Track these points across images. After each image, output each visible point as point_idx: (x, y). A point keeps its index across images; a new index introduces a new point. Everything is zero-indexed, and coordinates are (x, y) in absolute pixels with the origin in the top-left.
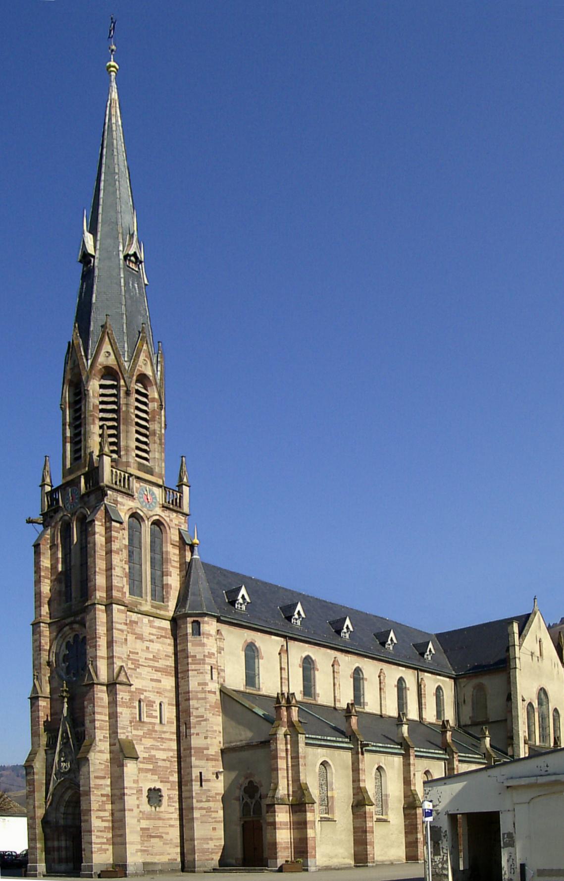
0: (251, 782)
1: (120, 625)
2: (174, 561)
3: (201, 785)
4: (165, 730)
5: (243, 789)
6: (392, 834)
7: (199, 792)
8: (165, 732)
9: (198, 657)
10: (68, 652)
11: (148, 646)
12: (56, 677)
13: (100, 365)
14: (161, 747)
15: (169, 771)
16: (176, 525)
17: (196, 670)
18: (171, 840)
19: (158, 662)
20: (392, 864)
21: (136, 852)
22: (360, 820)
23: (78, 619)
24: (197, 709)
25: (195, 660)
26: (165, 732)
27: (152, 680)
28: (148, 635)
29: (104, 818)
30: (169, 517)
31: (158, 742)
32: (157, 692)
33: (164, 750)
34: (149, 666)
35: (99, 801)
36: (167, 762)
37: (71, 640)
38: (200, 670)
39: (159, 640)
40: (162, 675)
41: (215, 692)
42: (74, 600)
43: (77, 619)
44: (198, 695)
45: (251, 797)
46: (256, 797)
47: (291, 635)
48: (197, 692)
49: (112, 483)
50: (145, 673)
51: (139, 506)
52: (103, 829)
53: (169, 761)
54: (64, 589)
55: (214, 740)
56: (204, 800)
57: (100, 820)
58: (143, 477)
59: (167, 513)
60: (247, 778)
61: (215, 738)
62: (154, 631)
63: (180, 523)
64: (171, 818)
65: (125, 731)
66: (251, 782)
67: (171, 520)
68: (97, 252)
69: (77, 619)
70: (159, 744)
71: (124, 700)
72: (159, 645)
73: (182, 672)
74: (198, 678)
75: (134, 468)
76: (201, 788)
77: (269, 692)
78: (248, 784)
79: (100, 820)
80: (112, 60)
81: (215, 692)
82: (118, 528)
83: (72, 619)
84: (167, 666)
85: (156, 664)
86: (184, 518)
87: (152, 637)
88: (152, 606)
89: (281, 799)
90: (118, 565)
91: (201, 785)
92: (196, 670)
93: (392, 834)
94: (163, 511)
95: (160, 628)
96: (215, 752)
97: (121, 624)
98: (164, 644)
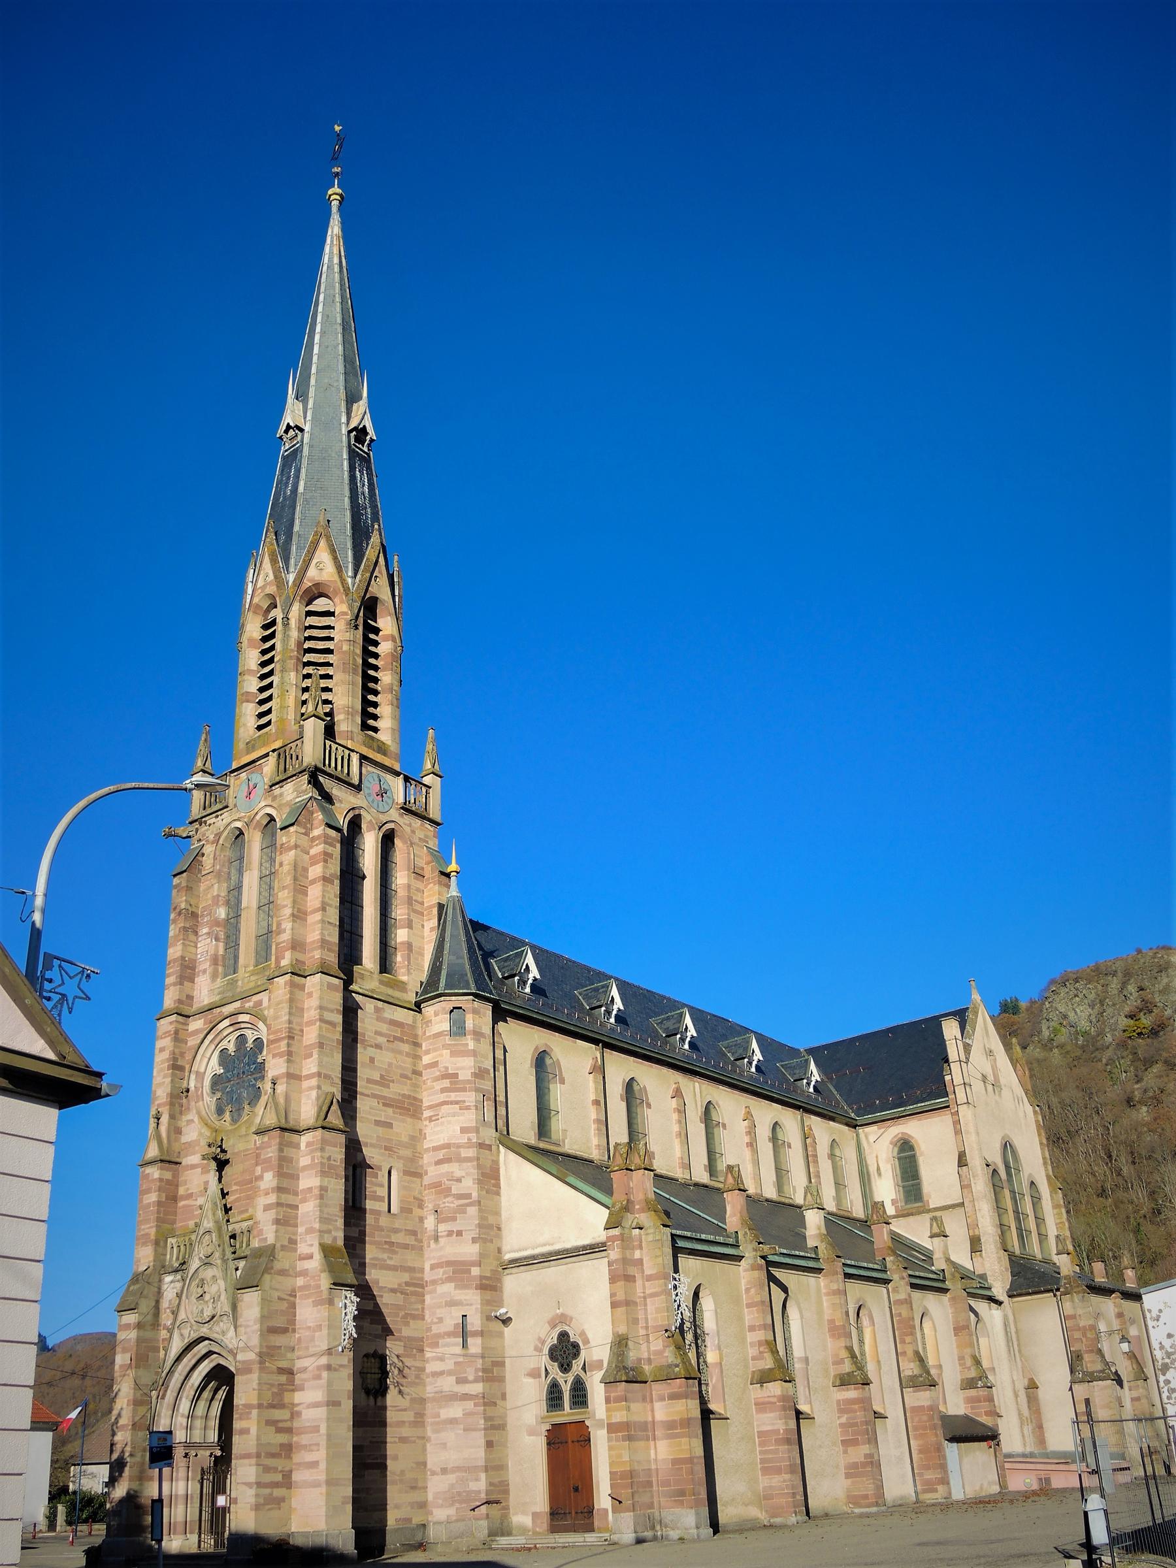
0: (563, 1336)
1: (330, 1014)
2: (416, 901)
3: (464, 1345)
4: (397, 1226)
5: (546, 1351)
6: (820, 1446)
7: (461, 1359)
8: (396, 1231)
9: (460, 1078)
10: (222, 1071)
11: (373, 1055)
12: (196, 1119)
13: (308, 580)
14: (389, 1262)
15: (402, 1313)
16: (420, 839)
17: (457, 1103)
18: (402, 1472)
19: (389, 1087)
20: (827, 1515)
21: (343, 1503)
22: (772, 1415)
23: (249, 1005)
24: (459, 1180)
25: (456, 1083)
26: (396, 1231)
27: (378, 1123)
28: (373, 1035)
29: (281, 1425)
30: (410, 825)
31: (384, 1250)
32: (386, 1148)
33: (394, 1268)
34: (374, 1096)
35: (272, 1385)
36: (398, 1294)
37: (231, 1048)
38: (464, 1101)
39: (390, 1045)
40: (394, 1113)
41: (491, 1146)
42: (241, 970)
43: (247, 1005)
44: (459, 1154)
45: (565, 1368)
46: (574, 1367)
47: (606, 1040)
48: (459, 1146)
49: (324, 765)
50: (367, 1108)
51: (364, 804)
52: (277, 1450)
53: (402, 1293)
54: (221, 951)
55: (488, 1244)
56: (471, 1378)
57: (273, 1429)
58: (371, 756)
59: (408, 819)
60: (554, 1327)
61: (491, 1241)
62: (384, 1028)
63: (426, 836)
64: (403, 1422)
65: (331, 1227)
66: (563, 1336)
67: (413, 832)
68: (308, 424)
69: (247, 1005)
70: (385, 1256)
71: (332, 1162)
72: (390, 1054)
73: (430, 1107)
74: (461, 1118)
75: (358, 741)
76: (463, 1352)
77: (575, 1147)
78: (559, 1338)
79: (273, 1429)
80: (336, 186)
81: (491, 1146)
82: (334, 838)
83: (237, 1005)
84: (404, 1095)
85: (385, 1092)
86: (432, 829)
87: (381, 1040)
88: (381, 982)
89: (632, 1369)
90: (331, 902)
91: (464, 1345)
92: (457, 1103)
93: (820, 1446)
94: (401, 815)
95: (393, 1023)
96: (492, 1270)
97: (332, 1011)
98: (400, 1052)
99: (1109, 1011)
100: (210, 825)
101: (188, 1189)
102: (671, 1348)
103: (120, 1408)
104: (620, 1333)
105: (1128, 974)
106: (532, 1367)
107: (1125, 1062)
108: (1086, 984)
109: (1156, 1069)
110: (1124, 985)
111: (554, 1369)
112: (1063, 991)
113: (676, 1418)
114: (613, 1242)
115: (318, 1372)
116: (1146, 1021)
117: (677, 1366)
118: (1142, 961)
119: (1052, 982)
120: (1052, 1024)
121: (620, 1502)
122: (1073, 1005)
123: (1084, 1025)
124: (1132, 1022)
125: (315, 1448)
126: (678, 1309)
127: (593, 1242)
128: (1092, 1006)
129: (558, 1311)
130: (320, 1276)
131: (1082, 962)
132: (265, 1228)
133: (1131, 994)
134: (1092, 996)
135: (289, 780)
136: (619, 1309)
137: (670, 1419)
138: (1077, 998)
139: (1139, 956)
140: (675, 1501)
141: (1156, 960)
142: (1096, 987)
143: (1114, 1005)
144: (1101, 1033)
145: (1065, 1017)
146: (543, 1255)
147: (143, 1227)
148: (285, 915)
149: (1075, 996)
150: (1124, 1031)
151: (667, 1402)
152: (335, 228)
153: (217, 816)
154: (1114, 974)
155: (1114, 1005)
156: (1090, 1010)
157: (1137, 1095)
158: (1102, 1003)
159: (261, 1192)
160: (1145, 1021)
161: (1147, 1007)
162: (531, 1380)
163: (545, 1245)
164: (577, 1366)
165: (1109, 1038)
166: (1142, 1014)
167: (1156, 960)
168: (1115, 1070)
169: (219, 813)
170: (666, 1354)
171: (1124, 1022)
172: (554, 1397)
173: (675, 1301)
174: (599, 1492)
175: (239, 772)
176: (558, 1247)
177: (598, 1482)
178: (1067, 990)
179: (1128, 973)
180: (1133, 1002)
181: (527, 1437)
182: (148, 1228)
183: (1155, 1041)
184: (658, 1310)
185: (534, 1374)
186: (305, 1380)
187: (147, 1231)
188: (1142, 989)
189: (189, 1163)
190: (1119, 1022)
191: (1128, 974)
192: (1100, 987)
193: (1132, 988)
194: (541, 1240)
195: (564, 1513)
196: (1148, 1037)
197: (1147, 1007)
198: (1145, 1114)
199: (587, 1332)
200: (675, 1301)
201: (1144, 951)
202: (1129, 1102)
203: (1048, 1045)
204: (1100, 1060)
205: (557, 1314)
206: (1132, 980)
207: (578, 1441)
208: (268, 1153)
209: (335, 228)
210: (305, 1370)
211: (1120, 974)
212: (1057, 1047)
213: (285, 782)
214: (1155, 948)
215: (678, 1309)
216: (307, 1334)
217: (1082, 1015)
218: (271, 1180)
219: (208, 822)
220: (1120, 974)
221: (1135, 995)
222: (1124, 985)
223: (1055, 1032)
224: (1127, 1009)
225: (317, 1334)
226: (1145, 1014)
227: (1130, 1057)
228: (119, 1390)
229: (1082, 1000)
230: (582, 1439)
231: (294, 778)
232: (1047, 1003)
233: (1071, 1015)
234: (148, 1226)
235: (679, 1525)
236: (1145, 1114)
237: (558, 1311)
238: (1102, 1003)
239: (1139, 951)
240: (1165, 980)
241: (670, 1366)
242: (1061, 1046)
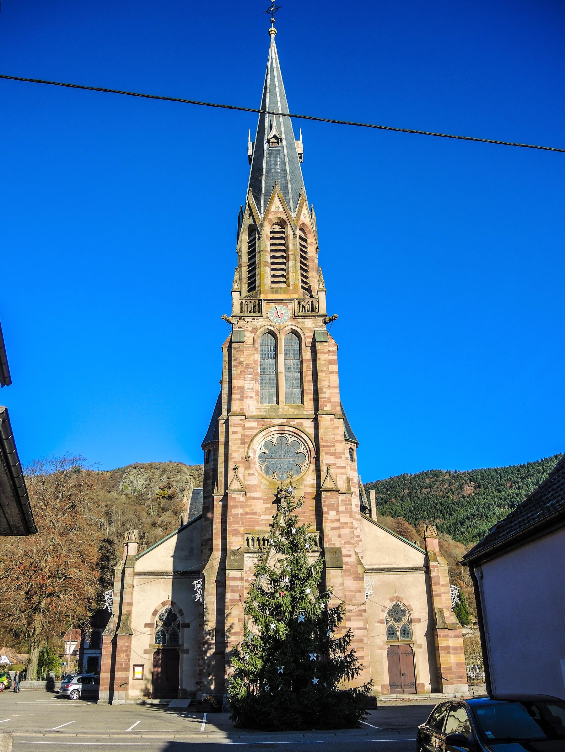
45: (398, 620)
99: (153, 484)
100: (248, 322)
101: (253, 510)
102: (454, 616)
103: (231, 622)
104: (439, 608)
105: (164, 470)
106: (380, 619)
107: (155, 508)
108: (145, 471)
109: (169, 513)
110: (162, 475)
111: (391, 622)
112: (134, 471)
113: (457, 646)
114: (434, 568)
115: (360, 613)
116: (167, 492)
117: (458, 624)
118: (171, 466)
119: (130, 466)
120: (125, 484)
121: (447, 680)
122: (137, 478)
123: (139, 487)
124: (160, 491)
125: (361, 650)
126: (454, 600)
127: (414, 566)
128: (145, 480)
129: (395, 595)
130: (357, 566)
131: (146, 461)
132: (333, 539)
133: (164, 479)
134: (147, 476)
135: (309, 317)
136: (438, 597)
137: (455, 646)
138: (139, 475)
139: (171, 464)
140: (458, 680)
141: (177, 468)
142: (149, 473)
143: (155, 482)
144: (146, 493)
145: (132, 482)
146: (388, 569)
147: (233, 525)
148: (325, 385)
149: (139, 474)
150: (157, 494)
151: (453, 639)
152: (273, 49)
153: (254, 319)
154: (158, 469)
155: (155, 482)
156: (144, 482)
157: (159, 522)
158: (150, 480)
159: (328, 520)
160: (167, 492)
161: (169, 486)
162: (379, 624)
163: (387, 564)
164: (405, 619)
165: (149, 496)
166: (166, 489)
167: (177, 468)
168: (150, 510)
169: (255, 318)
170: (451, 618)
171: (158, 490)
172: (391, 633)
173: (452, 596)
174: (419, 676)
175: (269, 301)
176: (394, 566)
177: (419, 672)
178: (136, 471)
179: (165, 470)
180: (164, 483)
181: (378, 650)
182: (238, 527)
183: (169, 502)
184: (447, 599)
185: (381, 622)
186: (351, 616)
187: (237, 528)
188: (169, 478)
189: (253, 496)
190: (156, 490)
191: (164, 470)
192: (151, 473)
193: (165, 477)
194: (384, 562)
195: (397, 685)
196: (166, 499)
197: (169, 486)
198: (160, 531)
199: (411, 606)
200: (452, 596)
201: (173, 462)
202: (154, 524)
203: (121, 493)
204: (144, 504)
205: (394, 596)
206: (166, 473)
207: (405, 654)
208: (331, 501)
209: (273, 49)
210: (350, 611)
211: (161, 470)
212: (125, 495)
213: (305, 317)
214: (177, 462)
215: (454, 600)
216: (350, 593)
217: (140, 484)
218: (334, 516)
219: (246, 320)
220: (161, 470)
221: (166, 480)
222: (162, 475)
223: (126, 488)
224: (160, 485)
225: (357, 594)
226: (167, 489)
227: (157, 506)
228: (230, 613)
229: (141, 477)
230: (407, 652)
231: (312, 317)
232: (125, 474)
233: (135, 482)
234: (237, 525)
235: (460, 691)
236: (160, 531)
237: (395, 595)
238: (150, 480)
239: (171, 462)
240: (179, 477)
241: (454, 624)
242: (127, 495)
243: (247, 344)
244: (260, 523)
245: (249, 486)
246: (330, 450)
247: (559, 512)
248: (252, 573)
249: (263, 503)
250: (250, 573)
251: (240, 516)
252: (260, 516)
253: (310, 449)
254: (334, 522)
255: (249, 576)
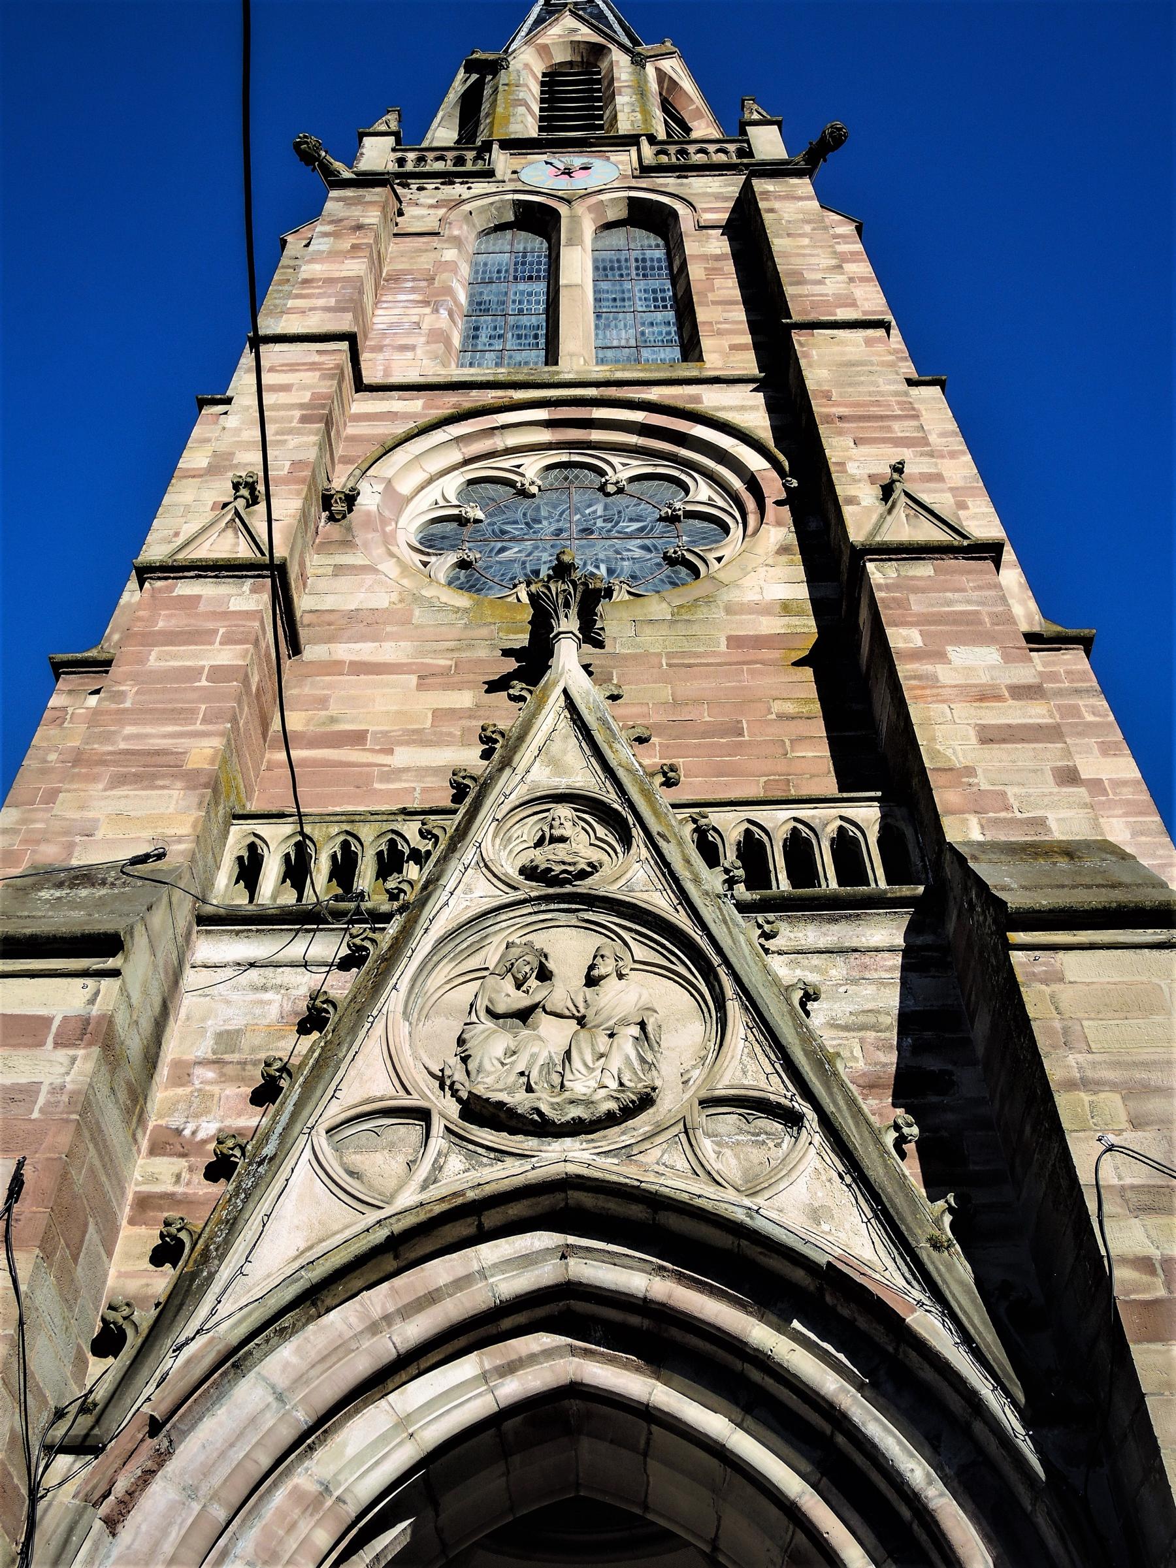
101: (333, 720)
132: (1011, 791)
243: (295, 1061)
244: (377, 786)
245: (331, 617)
246: (889, 429)
247: (480, 1226)
248: (241, 1080)
249: (420, 687)
250: (224, 1079)
251: (204, 683)
252: (391, 751)
253: (446, 983)
254: (998, 698)
255: (203, 1104)
